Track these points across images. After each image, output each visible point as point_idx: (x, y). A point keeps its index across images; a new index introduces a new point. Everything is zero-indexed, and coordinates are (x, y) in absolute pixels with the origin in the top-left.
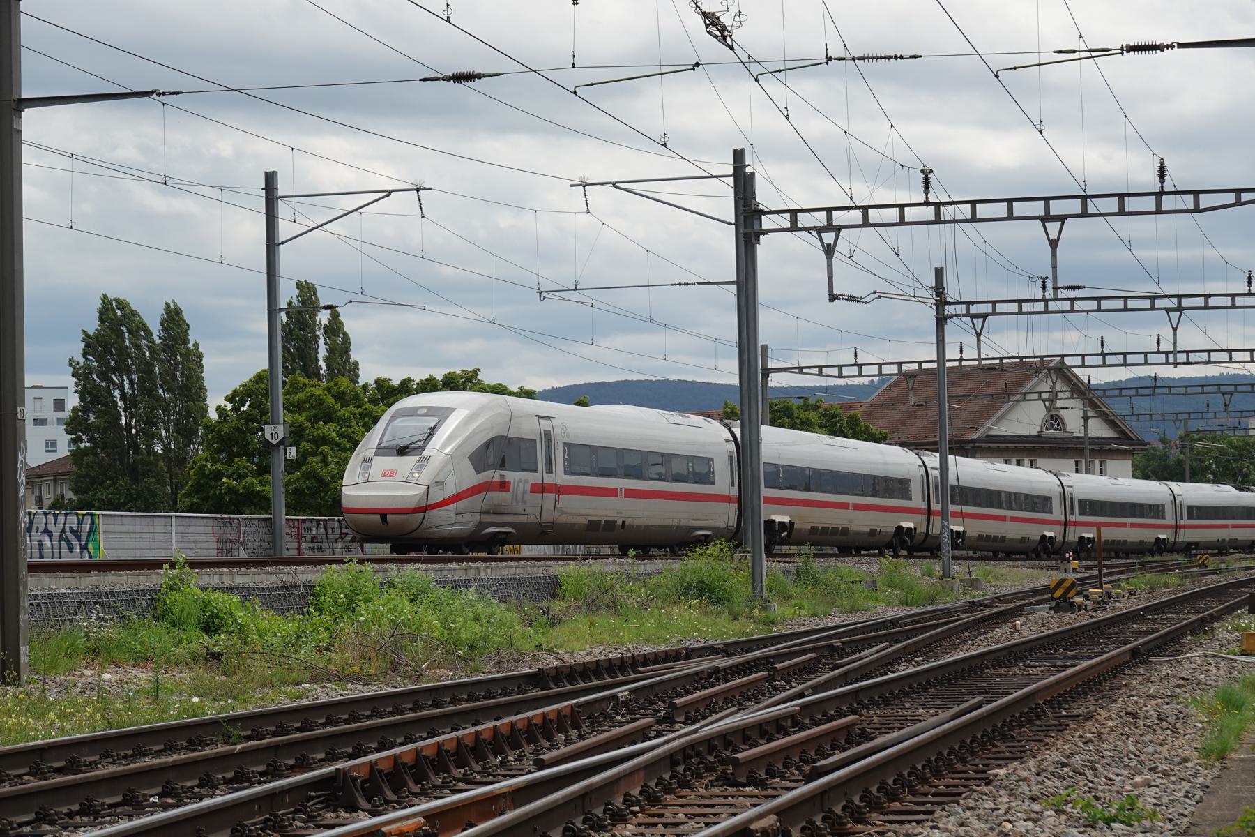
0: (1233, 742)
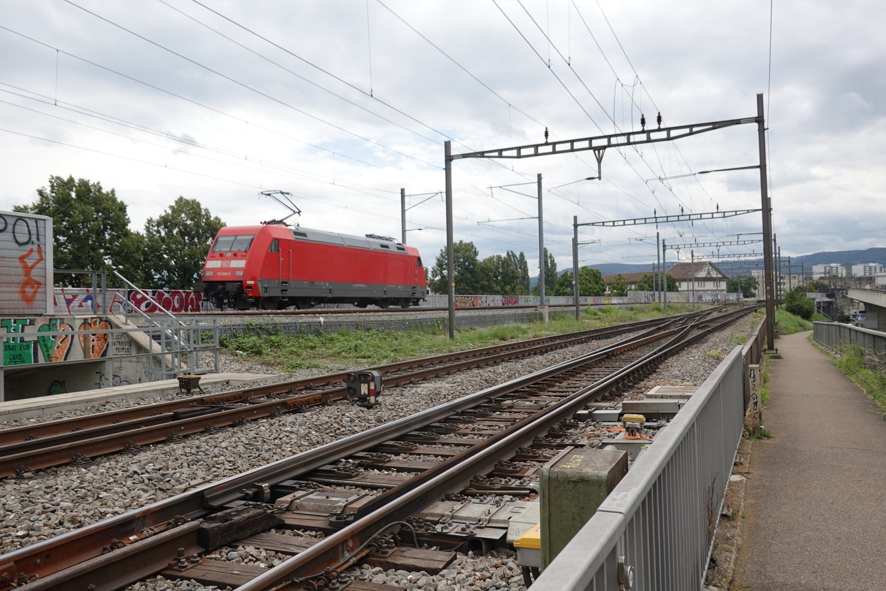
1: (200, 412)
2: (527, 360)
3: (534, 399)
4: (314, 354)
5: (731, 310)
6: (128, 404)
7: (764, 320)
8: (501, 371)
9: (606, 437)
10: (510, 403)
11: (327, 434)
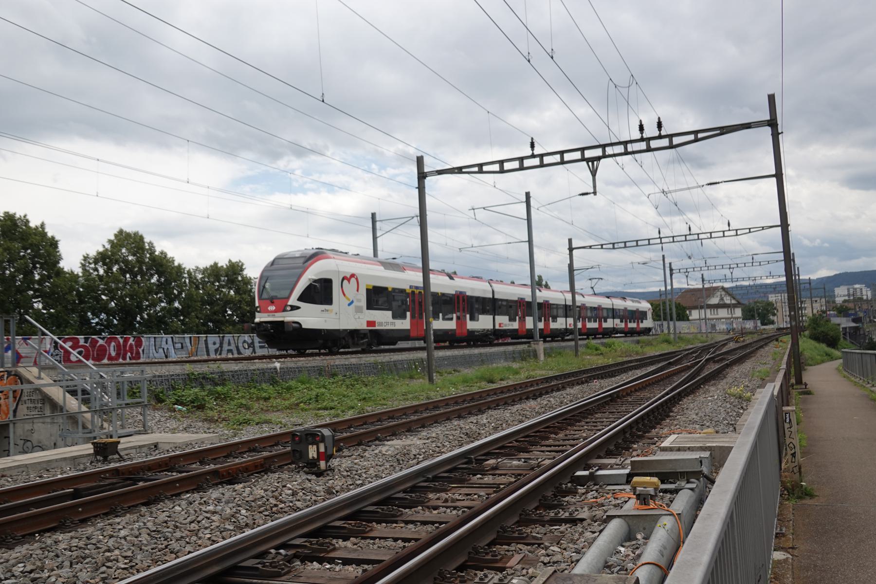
1: (108, 487)
2: (517, 406)
3: (523, 455)
4: (267, 407)
5: (749, 339)
6: (27, 477)
7: (788, 350)
8: (485, 421)
9: (612, 507)
10: (494, 464)
11: (260, 512)
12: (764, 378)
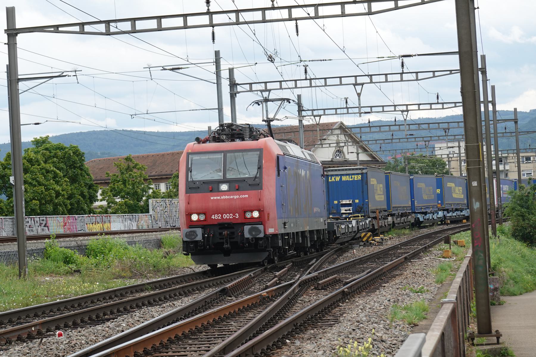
0: (444, 279)
7: (466, 262)
12: (416, 322)
